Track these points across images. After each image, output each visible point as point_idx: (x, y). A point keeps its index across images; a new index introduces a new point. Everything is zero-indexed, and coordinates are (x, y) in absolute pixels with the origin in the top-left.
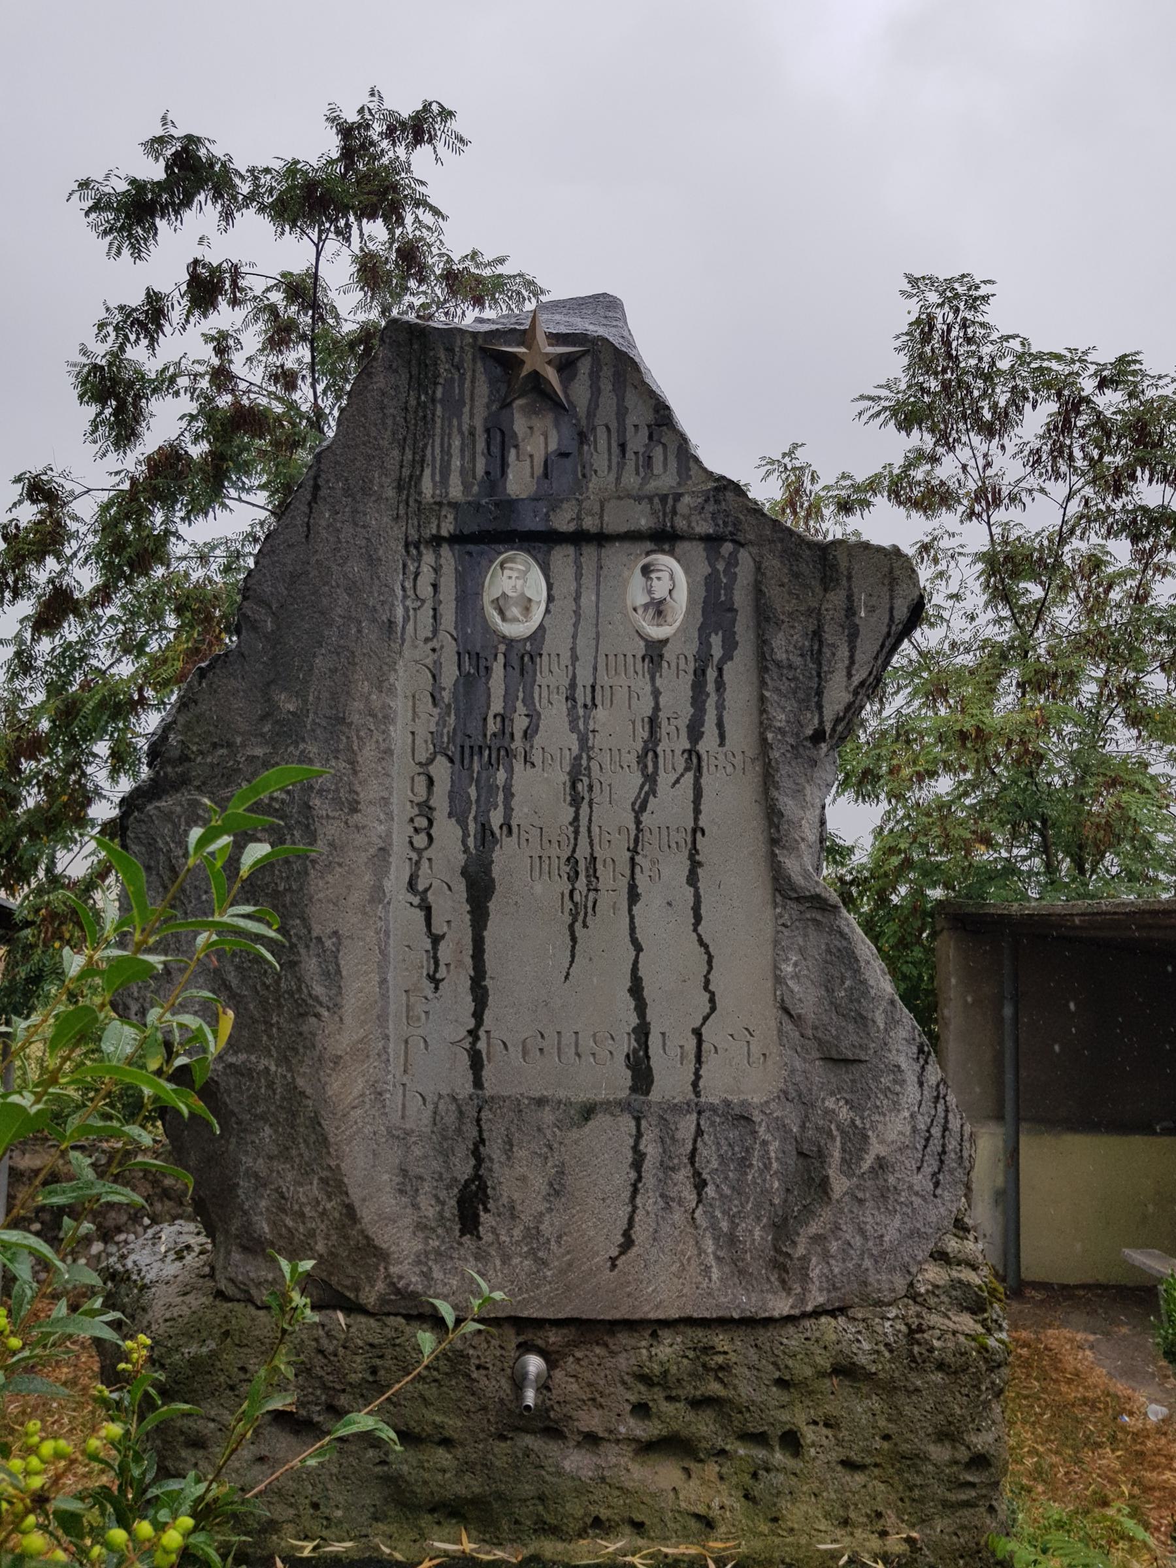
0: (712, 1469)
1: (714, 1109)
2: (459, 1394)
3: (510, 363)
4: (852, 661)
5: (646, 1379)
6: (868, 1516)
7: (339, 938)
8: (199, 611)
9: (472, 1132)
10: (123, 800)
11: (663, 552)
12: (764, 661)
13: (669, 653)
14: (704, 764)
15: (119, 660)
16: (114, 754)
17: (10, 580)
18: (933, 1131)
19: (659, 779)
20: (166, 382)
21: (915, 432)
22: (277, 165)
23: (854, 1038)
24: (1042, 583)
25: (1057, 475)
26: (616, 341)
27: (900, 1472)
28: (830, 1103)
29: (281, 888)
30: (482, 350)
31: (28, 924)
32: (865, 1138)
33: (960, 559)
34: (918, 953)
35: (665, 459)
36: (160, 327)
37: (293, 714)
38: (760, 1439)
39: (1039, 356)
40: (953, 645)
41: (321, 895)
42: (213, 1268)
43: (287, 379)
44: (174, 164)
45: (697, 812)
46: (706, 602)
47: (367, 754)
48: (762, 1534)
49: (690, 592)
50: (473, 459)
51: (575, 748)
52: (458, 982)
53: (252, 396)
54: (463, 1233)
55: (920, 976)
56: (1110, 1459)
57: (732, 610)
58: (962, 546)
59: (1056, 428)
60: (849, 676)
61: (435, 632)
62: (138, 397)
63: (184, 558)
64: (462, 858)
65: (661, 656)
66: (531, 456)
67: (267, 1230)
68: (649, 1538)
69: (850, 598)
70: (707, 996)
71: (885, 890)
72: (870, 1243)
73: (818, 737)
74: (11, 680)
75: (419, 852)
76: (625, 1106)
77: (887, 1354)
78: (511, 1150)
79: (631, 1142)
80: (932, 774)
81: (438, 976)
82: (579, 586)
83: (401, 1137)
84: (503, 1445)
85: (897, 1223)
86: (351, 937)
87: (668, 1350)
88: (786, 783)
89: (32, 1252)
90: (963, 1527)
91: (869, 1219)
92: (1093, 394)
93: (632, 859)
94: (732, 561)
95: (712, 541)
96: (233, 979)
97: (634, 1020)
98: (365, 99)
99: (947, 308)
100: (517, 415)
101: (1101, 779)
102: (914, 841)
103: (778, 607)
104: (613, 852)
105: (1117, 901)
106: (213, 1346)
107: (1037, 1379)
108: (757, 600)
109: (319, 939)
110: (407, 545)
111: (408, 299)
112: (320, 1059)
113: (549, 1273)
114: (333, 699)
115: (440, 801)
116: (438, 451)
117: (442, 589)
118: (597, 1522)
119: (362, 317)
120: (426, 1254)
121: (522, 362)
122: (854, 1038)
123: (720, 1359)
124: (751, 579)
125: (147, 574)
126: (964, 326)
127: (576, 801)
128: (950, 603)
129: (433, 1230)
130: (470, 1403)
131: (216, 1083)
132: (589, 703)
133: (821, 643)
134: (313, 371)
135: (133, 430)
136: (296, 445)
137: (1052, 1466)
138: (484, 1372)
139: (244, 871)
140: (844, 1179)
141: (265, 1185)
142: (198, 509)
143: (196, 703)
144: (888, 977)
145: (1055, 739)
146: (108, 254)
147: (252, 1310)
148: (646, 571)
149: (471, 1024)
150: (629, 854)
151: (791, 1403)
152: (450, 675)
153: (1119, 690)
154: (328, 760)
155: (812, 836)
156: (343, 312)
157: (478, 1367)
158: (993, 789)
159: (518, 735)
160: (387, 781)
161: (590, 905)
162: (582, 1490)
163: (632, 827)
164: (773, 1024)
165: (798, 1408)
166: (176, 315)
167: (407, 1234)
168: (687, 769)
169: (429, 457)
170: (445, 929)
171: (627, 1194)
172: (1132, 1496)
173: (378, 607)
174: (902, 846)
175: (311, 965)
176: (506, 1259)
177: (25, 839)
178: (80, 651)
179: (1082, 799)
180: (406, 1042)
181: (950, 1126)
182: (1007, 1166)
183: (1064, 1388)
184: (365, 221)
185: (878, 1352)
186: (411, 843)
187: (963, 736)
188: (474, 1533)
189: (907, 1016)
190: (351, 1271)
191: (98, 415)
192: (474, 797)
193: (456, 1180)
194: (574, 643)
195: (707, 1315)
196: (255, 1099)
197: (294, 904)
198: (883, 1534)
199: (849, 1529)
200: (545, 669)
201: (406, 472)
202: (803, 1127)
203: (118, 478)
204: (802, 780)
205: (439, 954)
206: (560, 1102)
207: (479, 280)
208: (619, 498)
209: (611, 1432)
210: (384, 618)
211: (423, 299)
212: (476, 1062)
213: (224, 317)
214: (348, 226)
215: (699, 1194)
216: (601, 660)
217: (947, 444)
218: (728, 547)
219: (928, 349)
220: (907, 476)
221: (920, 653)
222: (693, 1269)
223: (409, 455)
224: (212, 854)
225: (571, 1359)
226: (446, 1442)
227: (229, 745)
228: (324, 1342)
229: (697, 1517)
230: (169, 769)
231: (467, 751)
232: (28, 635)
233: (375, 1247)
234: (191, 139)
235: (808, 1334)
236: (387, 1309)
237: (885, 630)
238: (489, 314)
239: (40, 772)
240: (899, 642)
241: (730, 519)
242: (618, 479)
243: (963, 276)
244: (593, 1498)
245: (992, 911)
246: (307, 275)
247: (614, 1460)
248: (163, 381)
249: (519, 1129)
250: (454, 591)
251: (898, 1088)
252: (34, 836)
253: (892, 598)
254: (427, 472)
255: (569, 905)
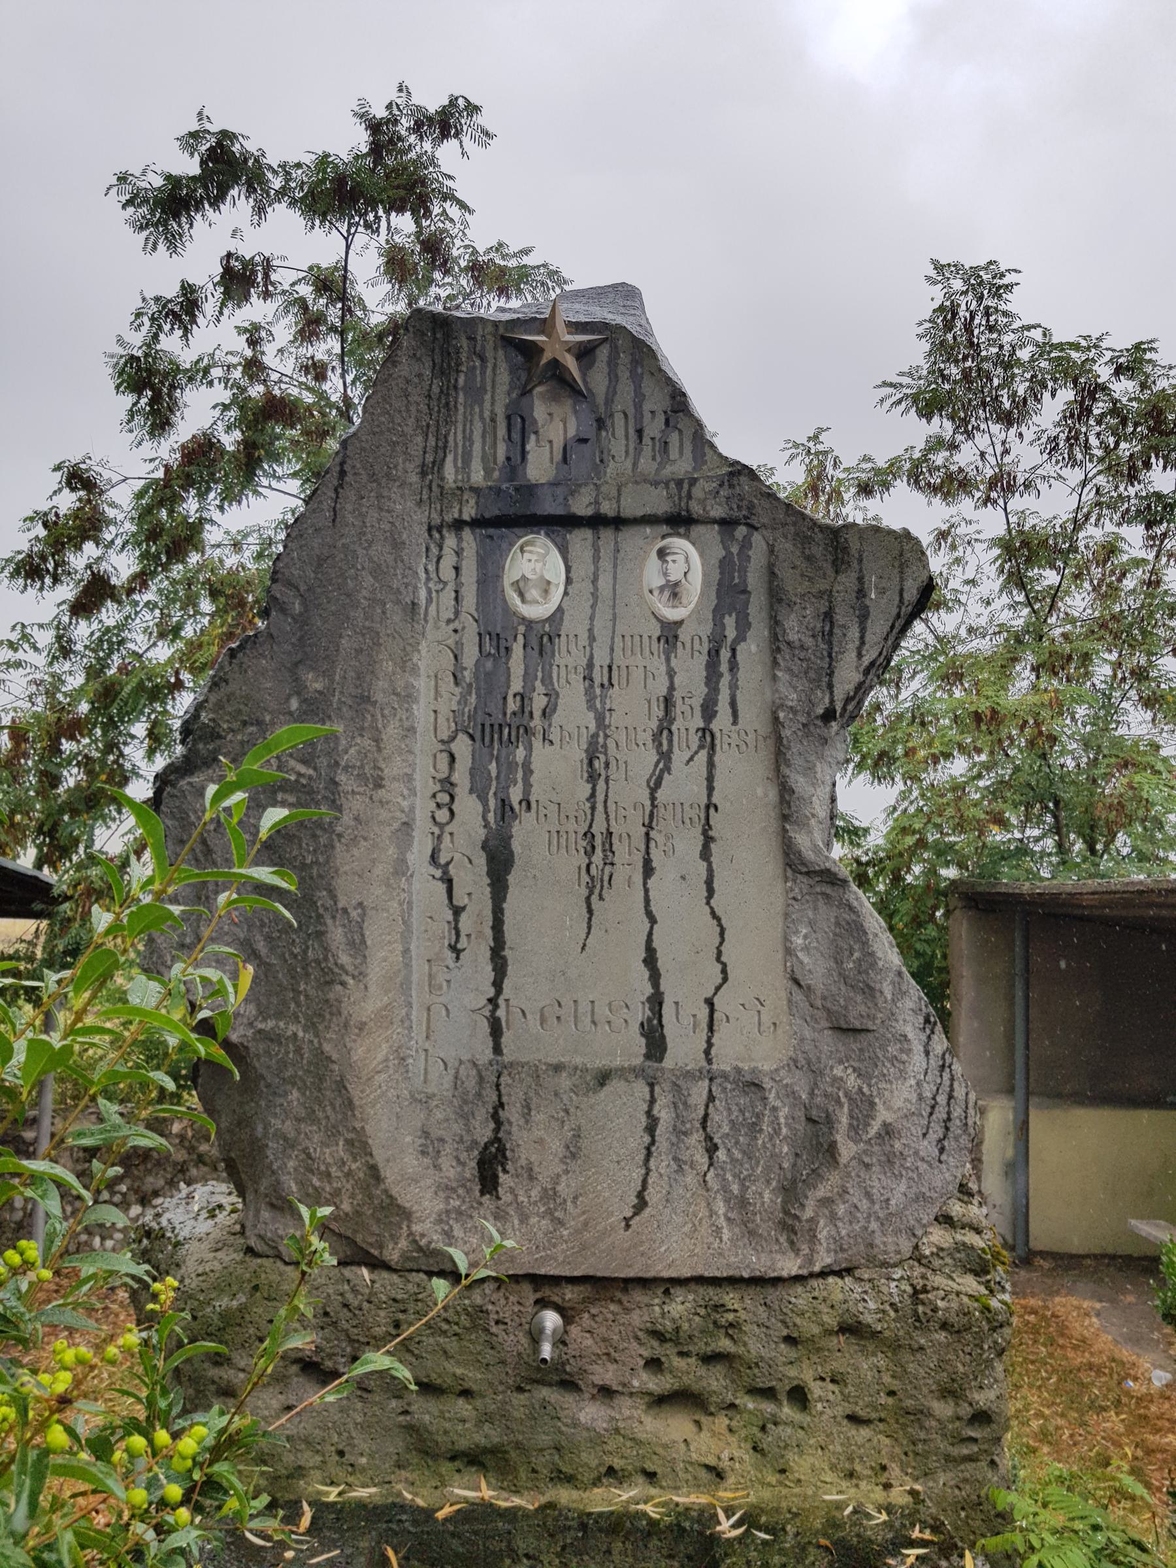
0: (722, 1421)
1: (725, 1076)
2: (479, 1348)
3: (530, 351)
4: (863, 643)
5: (658, 1335)
6: (872, 1468)
7: (363, 909)
8: (232, 596)
9: (491, 1097)
10: (156, 777)
11: (679, 535)
12: (776, 643)
13: (684, 634)
14: (717, 742)
15: (155, 644)
16: (151, 734)
17: (51, 566)
18: (939, 1099)
19: (674, 757)
20: (200, 373)
21: (936, 420)
22: (308, 159)
23: (862, 1009)
24: (1058, 570)
25: (1074, 463)
26: (634, 329)
27: (904, 1426)
28: (838, 1071)
29: (308, 861)
30: (503, 338)
31: (67, 898)
32: (872, 1105)
33: (977, 545)
34: (931, 931)
35: (681, 445)
36: (193, 321)
37: (320, 693)
38: (768, 1393)
39: (1060, 346)
40: (970, 630)
41: (347, 868)
42: (243, 1226)
43: (318, 371)
44: (209, 158)
45: (710, 789)
46: (720, 584)
47: (391, 732)
48: (769, 1485)
49: (704, 575)
50: (494, 445)
51: (593, 726)
52: (479, 952)
53: (283, 386)
54: (482, 1193)
55: (934, 955)
56: (1114, 1421)
57: (745, 592)
58: (979, 532)
59: (1072, 416)
60: (860, 656)
61: (457, 613)
62: (173, 387)
63: (219, 546)
64: (482, 833)
65: (676, 637)
66: (550, 442)
67: (294, 1188)
68: (662, 1487)
69: (860, 579)
70: (719, 967)
71: (899, 870)
72: (877, 1207)
73: (829, 716)
74: (51, 664)
75: (441, 826)
76: (639, 1072)
77: (892, 1314)
78: (529, 1114)
79: (645, 1107)
80: (947, 756)
81: (459, 946)
82: (597, 569)
83: (423, 1101)
84: (522, 1397)
85: (903, 1188)
86: (375, 908)
87: (680, 1307)
88: (797, 761)
89: (59, 1184)
90: (965, 1480)
91: (876, 1184)
92: (1109, 381)
93: (647, 834)
94: (746, 544)
95: (727, 524)
96: (261, 946)
97: (649, 990)
98: (393, 95)
99: (970, 296)
100: (537, 402)
101: (1113, 760)
102: (929, 821)
103: (790, 588)
104: (630, 826)
105: (1126, 880)
106: (244, 1300)
107: (1045, 1345)
108: (770, 582)
109: (345, 910)
110: (430, 529)
111: (433, 290)
112: (346, 1025)
113: (565, 1233)
114: (358, 678)
115: (461, 777)
116: (460, 436)
117: (464, 571)
118: (611, 1471)
119: (390, 309)
120: (448, 1212)
121: (542, 350)
122: (862, 1009)
123: (730, 1317)
124: (764, 562)
125: (183, 562)
126: (987, 314)
127: (593, 778)
128: (967, 588)
129: (454, 1190)
130: (490, 1356)
131: (246, 1048)
132: (606, 682)
133: (832, 623)
134: (343, 362)
135: (168, 419)
136: (324, 435)
137: (1057, 1428)
138: (502, 1327)
139: (263, 834)
140: (851, 1144)
141: (293, 1147)
142: (230, 497)
143: (226, 681)
144: (896, 950)
145: (1068, 722)
146: (144, 249)
147: (279, 1264)
148: (662, 554)
149: (491, 992)
150: (644, 830)
151: (799, 1359)
152: (470, 655)
153: (1132, 673)
154: (353, 738)
155: (822, 812)
156: (370, 304)
157: (497, 1322)
158: (1006, 772)
159: (537, 714)
160: (411, 758)
161: (606, 878)
162: (597, 1440)
163: (648, 803)
164: (783, 994)
165: (805, 1364)
166: (210, 307)
167: (429, 1194)
168: (701, 747)
169: (451, 443)
170: (466, 901)
171: (641, 1157)
172: (1135, 1458)
173: (402, 589)
174: (917, 826)
175: (337, 935)
176: (524, 1219)
177: (66, 818)
178: (118, 635)
179: (1094, 781)
180: (429, 1009)
181: (955, 1094)
182: (1018, 1139)
183: (1071, 1354)
184: (393, 214)
185: (884, 1312)
186: (433, 818)
187: (978, 717)
188: (493, 1481)
189: (914, 990)
190: (375, 1229)
191: (134, 405)
192: (494, 774)
193: (476, 1142)
194: (592, 624)
195: (718, 1274)
196: (283, 1064)
197: (320, 876)
198: (887, 1486)
199: (854, 1481)
200: (564, 648)
201: (430, 458)
202: (812, 1094)
203: (152, 466)
204: (813, 758)
205: (460, 925)
206: (576, 1068)
207: (503, 270)
208: (637, 483)
209: (624, 1385)
210: (408, 600)
211: (449, 291)
212: (496, 1030)
213: (257, 310)
214: (377, 217)
215: (711, 1158)
216: (618, 639)
217: (966, 431)
218: (741, 531)
219: (950, 336)
220: (926, 461)
221: (937, 637)
222: (704, 1230)
223: (432, 441)
224: (228, 810)
225: (586, 1315)
226: (466, 1393)
227: (259, 723)
228: (350, 1296)
229: (709, 1468)
230: (201, 746)
231: (488, 729)
232: (66, 619)
233: (399, 1206)
234: (225, 135)
235: (816, 1294)
236: (409, 1265)
237: (895, 611)
238: (514, 303)
239: (79, 753)
240: (908, 624)
241: (745, 503)
242: (635, 465)
243: (990, 263)
244: (607, 1448)
245: (1003, 890)
246: (336, 269)
247: (627, 1413)
248: (198, 371)
249: (537, 1093)
250: (475, 574)
251: (904, 1057)
252: (74, 813)
253: (902, 580)
254: (450, 458)
255: (585, 878)
